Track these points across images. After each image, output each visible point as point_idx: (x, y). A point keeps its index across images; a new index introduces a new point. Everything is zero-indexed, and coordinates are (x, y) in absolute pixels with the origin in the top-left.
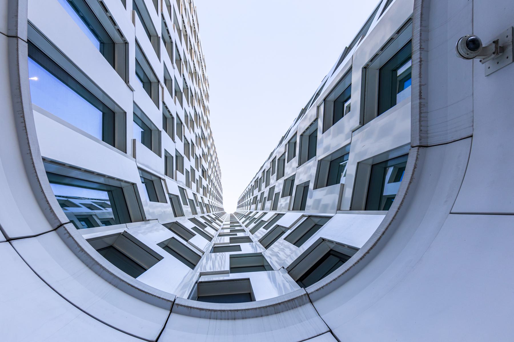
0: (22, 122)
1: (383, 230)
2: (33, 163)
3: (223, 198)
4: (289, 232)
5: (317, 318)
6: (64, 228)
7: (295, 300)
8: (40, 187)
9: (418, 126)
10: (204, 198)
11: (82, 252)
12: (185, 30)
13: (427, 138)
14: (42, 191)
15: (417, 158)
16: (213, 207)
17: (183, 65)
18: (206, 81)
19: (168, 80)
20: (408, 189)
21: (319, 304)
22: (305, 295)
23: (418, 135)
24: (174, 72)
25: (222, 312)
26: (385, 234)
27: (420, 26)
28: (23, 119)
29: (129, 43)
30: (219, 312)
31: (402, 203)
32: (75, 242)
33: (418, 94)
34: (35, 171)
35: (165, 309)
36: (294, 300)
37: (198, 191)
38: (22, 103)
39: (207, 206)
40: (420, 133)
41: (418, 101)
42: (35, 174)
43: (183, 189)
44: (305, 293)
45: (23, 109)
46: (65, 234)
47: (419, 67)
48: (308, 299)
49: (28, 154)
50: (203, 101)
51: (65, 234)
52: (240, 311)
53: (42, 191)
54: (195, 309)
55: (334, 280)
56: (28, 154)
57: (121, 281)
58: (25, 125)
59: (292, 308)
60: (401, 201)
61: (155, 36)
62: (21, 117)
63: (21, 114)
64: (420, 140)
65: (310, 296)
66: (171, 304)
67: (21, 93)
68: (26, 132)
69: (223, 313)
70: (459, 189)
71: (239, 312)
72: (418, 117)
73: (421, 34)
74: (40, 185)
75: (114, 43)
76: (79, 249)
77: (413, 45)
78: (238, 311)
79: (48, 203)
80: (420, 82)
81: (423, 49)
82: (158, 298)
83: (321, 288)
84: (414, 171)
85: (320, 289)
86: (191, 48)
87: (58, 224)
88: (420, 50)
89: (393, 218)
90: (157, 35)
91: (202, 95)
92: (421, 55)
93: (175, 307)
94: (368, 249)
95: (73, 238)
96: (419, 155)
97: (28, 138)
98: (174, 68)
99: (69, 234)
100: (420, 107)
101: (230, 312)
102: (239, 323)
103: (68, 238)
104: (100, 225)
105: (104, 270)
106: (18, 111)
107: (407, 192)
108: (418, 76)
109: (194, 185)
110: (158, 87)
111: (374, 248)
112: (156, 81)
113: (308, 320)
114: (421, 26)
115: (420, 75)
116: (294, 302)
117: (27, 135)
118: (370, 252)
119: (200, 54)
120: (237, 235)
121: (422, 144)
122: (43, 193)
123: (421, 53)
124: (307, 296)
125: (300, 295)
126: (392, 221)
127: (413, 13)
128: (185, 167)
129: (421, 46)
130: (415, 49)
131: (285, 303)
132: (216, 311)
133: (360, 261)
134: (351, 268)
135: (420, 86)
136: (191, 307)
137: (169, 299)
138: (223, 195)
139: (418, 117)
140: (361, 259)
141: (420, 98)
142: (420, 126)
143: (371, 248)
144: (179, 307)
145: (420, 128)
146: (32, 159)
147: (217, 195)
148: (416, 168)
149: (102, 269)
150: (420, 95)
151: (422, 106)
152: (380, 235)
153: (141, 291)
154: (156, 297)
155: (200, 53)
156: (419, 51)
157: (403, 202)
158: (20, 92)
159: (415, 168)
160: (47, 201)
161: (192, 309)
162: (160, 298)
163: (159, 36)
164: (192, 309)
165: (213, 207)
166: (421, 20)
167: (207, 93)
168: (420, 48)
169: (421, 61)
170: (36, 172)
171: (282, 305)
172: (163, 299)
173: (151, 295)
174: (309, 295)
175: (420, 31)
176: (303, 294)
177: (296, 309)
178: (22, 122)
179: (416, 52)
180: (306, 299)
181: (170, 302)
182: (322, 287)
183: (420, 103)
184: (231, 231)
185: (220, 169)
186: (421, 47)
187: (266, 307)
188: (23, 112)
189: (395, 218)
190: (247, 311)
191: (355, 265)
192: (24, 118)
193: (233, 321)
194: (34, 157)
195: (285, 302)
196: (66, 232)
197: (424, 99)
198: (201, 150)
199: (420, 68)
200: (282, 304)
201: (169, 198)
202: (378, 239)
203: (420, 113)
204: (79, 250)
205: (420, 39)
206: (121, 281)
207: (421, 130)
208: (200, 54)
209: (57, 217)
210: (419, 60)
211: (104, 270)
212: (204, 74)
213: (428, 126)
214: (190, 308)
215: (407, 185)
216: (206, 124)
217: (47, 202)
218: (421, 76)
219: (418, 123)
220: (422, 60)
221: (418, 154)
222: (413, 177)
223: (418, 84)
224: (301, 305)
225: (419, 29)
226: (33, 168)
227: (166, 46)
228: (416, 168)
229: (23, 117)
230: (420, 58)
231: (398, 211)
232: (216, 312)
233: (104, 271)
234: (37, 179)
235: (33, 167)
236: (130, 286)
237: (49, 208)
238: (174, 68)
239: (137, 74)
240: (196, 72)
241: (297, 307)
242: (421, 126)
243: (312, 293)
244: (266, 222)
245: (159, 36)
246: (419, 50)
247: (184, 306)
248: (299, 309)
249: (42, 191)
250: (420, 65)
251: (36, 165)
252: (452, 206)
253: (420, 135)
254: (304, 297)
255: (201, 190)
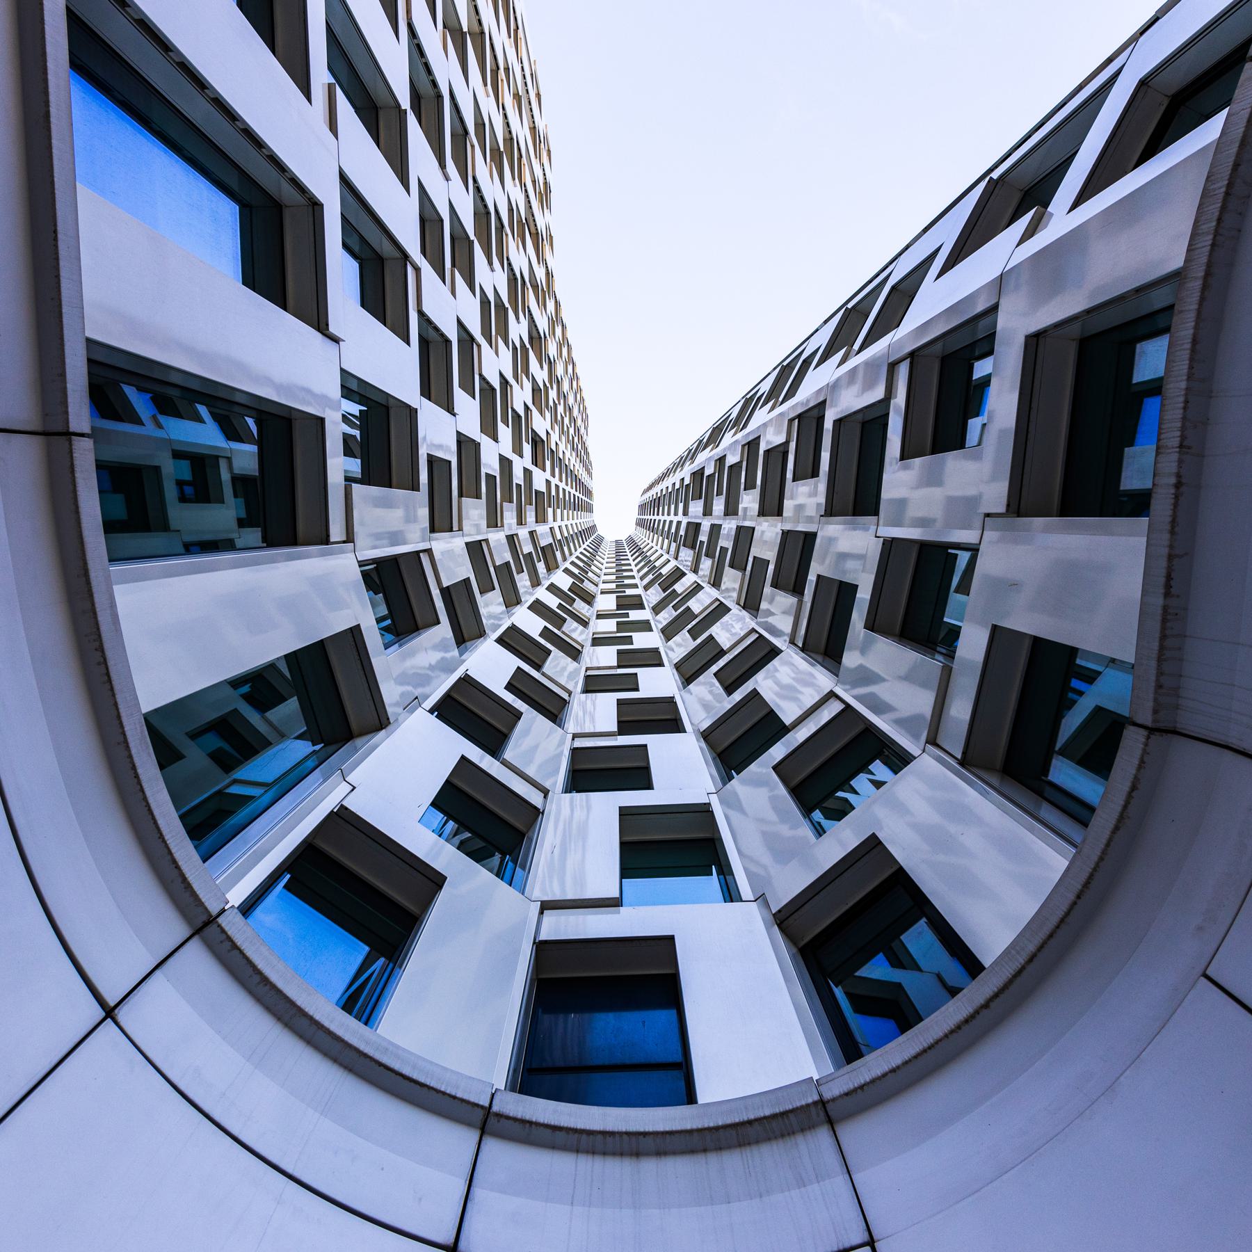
0: (99, 664)
1: (1031, 948)
2: (134, 768)
3: (594, 472)
4: (793, 446)
5: (841, 1181)
6: (219, 928)
7: (790, 1115)
8: (154, 826)
9: (1153, 672)
10: (536, 471)
11: (266, 985)
12: (477, 18)
13: (1177, 707)
14: (161, 836)
15: (1142, 762)
16: (557, 462)
17: (473, 146)
18: (542, 144)
19: (431, 221)
20: (1108, 845)
21: (852, 1133)
22: (815, 1103)
23: (1151, 696)
24: (488, 106)
25: (608, 1137)
26: (1035, 960)
27: (1185, 378)
28: (101, 654)
29: (323, 205)
30: (600, 1137)
31: (1090, 883)
32: (246, 961)
33: (1162, 580)
34: (139, 787)
35: (469, 1124)
36: (787, 1116)
37: (518, 451)
38: (95, 613)
39: (537, 442)
40: (1156, 692)
41: (1159, 601)
42: (141, 793)
43: (472, 339)
44: (816, 1098)
45: (98, 629)
46: (221, 942)
47: (1172, 501)
48: (822, 1114)
49: (119, 744)
50: (534, 220)
51: (221, 942)
52: (652, 1136)
53: (160, 838)
54: (542, 1128)
55: (893, 1071)
56: (119, 744)
57: (360, 1056)
58: (107, 668)
59: (783, 1136)
60: (1088, 875)
61: (394, 107)
62: (96, 650)
63: (94, 640)
64: (1155, 712)
65: (829, 1107)
66: (481, 1113)
67: (91, 587)
68: (109, 687)
69: (609, 1139)
70: (1239, 903)
71: (649, 1139)
72: (1155, 646)
73: (1186, 402)
74: (155, 822)
75: (281, 206)
76: (257, 978)
77: (1168, 387)
78: (647, 1137)
79: (176, 867)
80: (1171, 547)
81: (1189, 448)
82: (451, 1099)
83: (859, 1090)
84: (1130, 796)
85: (855, 1090)
86: (495, 68)
87: (204, 918)
88: (1179, 452)
89: (1062, 921)
90: (399, 106)
91: (529, 202)
92: (1180, 467)
93: (492, 1121)
94: (988, 996)
95: (241, 952)
96: (1148, 754)
97: (116, 704)
98: (447, 179)
99: (230, 943)
100: (1164, 621)
101: (625, 1137)
102: (649, 1166)
103: (229, 951)
104: (225, 500)
105: (319, 1028)
106: (86, 636)
107: (1104, 852)
108: (1168, 527)
109: (505, 432)
110: (403, 273)
111: (1002, 996)
112: (397, 254)
113: (818, 1182)
114: (1190, 377)
115: (1173, 527)
116: (786, 1120)
117: (114, 695)
118: (992, 1005)
119: (522, 67)
120: (628, 617)
121: (1161, 725)
122: (164, 841)
123: (1180, 462)
124: (820, 1106)
125: (803, 1103)
126: (1058, 927)
127: (1182, 268)
128: (475, 405)
129: (1183, 437)
130: (1165, 441)
131: (765, 1121)
132: (593, 1134)
133: (963, 1028)
134: (940, 1043)
135: (1170, 557)
136: (530, 1123)
137: (476, 1102)
138: (593, 485)
139: (1155, 645)
140: (966, 1021)
141: (1167, 594)
142: (1160, 673)
143: (996, 995)
144: (503, 1120)
145: (1157, 680)
146: (130, 756)
147: (573, 491)
148: (1137, 789)
149: (314, 1028)
150: (1168, 586)
151: (1169, 617)
152: (1022, 960)
153: (410, 1082)
154: (446, 1097)
155: (521, 63)
156: (1176, 452)
157: (1092, 879)
158: (88, 582)
159: (1134, 788)
160: (174, 862)
161: (533, 1126)
162: (454, 1097)
163: (403, 108)
164: (533, 1126)
165: (557, 462)
166: (1191, 359)
167: (546, 183)
168: (1181, 446)
169: (1178, 486)
170: (142, 790)
171: (756, 1125)
172: (462, 1100)
173: (435, 1092)
174: (826, 1105)
175: (1186, 395)
176: (810, 1101)
177: (790, 1142)
178: (99, 664)
179: (1170, 451)
180: (818, 1115)
181: (480, 1109)
182: (861, 1087)
183: (1165, 609)
184: (617, 577)
185: (583, 395)
186: (1184, 444)
187: (717, 1128)
188: (100, 636)
189: (1066, 920)
190: (668, 1136)
191: (949, 1036)
192: (103, 651)
193: (634, 1159)
194: (134, 751)
195: (765, 1118)
196: (224, 936)
197: (1178, 596)
198: (524, 323)
199: (1176, 505)
200: (757, 1123)
201: (428, 461)
202: (1016, 973)
203: (1163, 637)
204: (258, 981)
205: (1184, 419)
206: (360, 1056)
207: (1159, 686)
208: (522, 67)
209: (200, 900)
210: (1173, 480)
211: (319, 1028)
212: (535, 127)
213: (1181, 676)
214: (528, 1125)
215: (1106, 834)
216: (543, 289)
217: (173, 864)
218: (1176, 529)
219: (1154, 663)
220: (1184, 481)
221: (1145, 752)
222: (1125, 814)
223: (1165, 551)
224: (806, 1129)
225: (1183, 385)
226: (136, 780)
227: (423, 123)
228: (1137, 789)
229: (101, 649)
230: (1178, 476)
231: (1075, 903)
232: (591, 1136)
233: (320, 1033)
234: (147, 808)
235: (135, 777)
236: (382, 1067)
237: (180, 880)
238: (447, 179)
239: (345, 246)
240: (512, 139)
241: (794, 1133)
242: (1162, 674)
243: (834, 1100)
244: (715, 473)
245: (403, 108)
246: (1177, 450)
247: (515, 1119)
248: (800, 1139)
249: (160, 838)
250: (1177, 497)
251: (140, 771)
252: (1212, 953)
253: (1155, 700)
254: (813, 1109)
255: (527, 448)
